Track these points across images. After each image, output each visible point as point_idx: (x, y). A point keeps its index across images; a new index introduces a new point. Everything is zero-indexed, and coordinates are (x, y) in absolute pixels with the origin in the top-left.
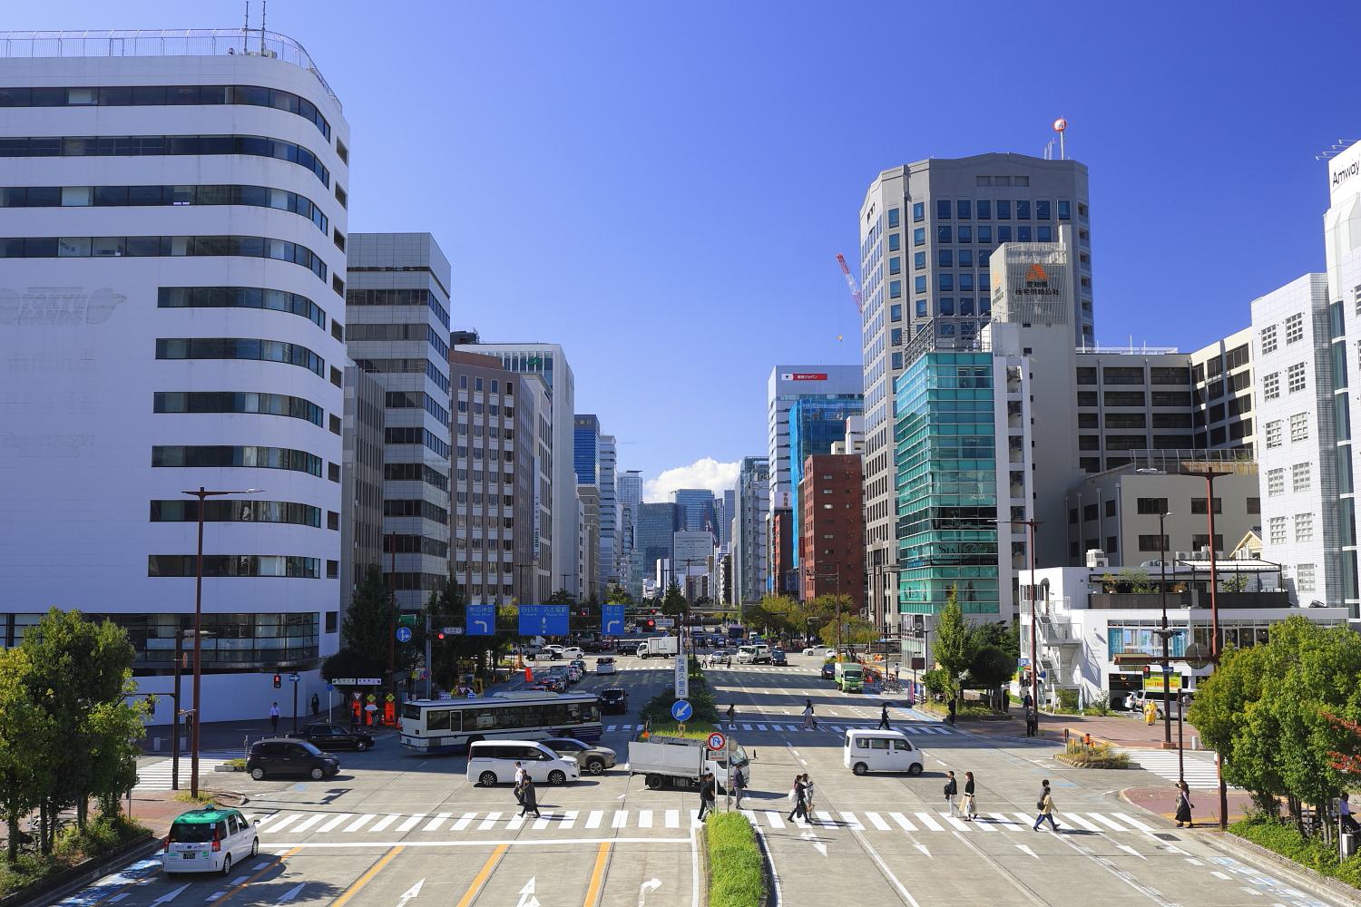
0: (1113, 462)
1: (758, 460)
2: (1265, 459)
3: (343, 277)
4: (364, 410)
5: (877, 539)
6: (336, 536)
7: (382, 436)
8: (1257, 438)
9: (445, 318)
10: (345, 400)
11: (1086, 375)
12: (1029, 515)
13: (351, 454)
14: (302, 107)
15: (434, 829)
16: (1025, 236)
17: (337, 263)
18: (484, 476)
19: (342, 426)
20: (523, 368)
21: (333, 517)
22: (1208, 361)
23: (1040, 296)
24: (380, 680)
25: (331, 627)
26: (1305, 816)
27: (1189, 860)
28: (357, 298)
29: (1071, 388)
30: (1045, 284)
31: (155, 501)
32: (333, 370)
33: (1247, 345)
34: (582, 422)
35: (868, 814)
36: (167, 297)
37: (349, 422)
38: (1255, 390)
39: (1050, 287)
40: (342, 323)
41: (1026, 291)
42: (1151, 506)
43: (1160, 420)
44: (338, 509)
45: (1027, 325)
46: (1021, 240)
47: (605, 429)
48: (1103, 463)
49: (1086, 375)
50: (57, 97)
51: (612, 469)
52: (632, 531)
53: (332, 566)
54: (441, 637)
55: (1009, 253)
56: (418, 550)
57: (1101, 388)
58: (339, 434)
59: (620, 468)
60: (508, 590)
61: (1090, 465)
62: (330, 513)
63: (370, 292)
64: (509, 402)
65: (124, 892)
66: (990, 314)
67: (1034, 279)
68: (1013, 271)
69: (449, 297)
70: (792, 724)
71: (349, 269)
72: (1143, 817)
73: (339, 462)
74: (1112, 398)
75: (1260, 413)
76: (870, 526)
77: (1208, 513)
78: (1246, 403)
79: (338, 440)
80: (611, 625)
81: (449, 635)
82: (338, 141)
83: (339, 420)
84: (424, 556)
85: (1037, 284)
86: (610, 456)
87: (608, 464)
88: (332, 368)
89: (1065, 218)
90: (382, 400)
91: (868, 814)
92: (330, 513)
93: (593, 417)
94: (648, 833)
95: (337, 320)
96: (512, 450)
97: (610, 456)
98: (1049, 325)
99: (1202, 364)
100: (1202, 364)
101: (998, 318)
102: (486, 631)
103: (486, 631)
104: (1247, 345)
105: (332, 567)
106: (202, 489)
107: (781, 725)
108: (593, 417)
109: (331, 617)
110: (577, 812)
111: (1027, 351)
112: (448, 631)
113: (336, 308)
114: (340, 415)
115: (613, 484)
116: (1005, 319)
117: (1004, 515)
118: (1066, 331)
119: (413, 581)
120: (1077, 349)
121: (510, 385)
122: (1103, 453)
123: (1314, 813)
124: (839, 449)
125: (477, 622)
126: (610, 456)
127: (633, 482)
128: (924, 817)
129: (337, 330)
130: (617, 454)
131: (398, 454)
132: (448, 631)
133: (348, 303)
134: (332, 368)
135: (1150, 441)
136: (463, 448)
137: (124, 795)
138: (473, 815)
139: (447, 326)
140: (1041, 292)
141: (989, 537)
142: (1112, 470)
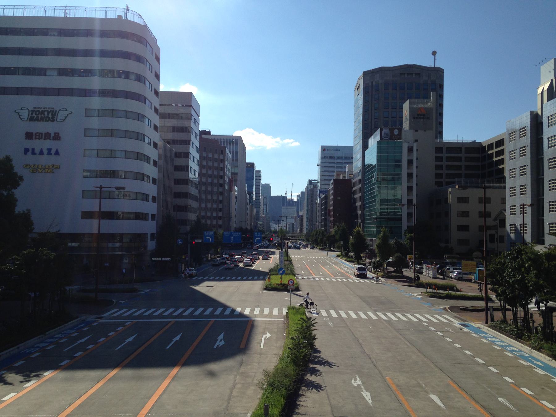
1: (313, 180)
2: (509, 183)
3: (158, 107)
6: (155, 205)
8: (507, 174)
9: (198, 124)
11: (439, 150)
12: (415, 202)
14: (122, 35)
15: (208, 314)
16: (417, 97)
17: (156, 102)
18: (211, 193)
20: (227, 145)
21: (154, 198)
22: (495, 142)
23: (422, 120)
24: (170, 258)
25: (152, 239)
26: (519, 320)
27: (472, 334)
28: (163, 116)
33: (504, 139)
34: (249, 165)
35: (349, 312)
37: (160, 163)
38: (506, 156)
40: (158, 125)
41: (417, 118)
42: (462, 200)
43: (467, 167)
44: (156, 195)
45: (416, 131)
46: (416, 98)
47: (258, 167)
52: (267, 206)
54: (194, 243)
55: (410, 103)
56: (186, 211)
58: (156, 167)
59: (263, 182)
60: (220, 226)
61: (439, 184)
62: (153, 197)
63: (169, 114)
64: (222, 157)
65: (39, 352)
66: (402, 127)
68: (411, 110)
69: (199, 117)
70: (322, 278)
71: (160, 105)
72: (456, 317)
75: (508, 166)
77: (483, 203)
78: (502, 161)
80: (257, 240)
81: (197, 242)
82: (156, 54)
83: (157, 162)
84: (189, 213)
86: (259, 178)
87: (258, 181)
89: (433, 90)
91: (349, 312)
93: (253, 163)
96: (222, 175)
97: (259, 178)
98: (425, 131)
99: (493, 143)
100: (493, 143)
101: (405, 128)
102: (210, 241)
103: (210, 241)
104: (504, 139)
105: (153, 216)
106: (101, 186)
107: (324, 278)
108: (253, 163)
110: (241, 308)
111: (416, 141)
112: (196, 241)
113: (156, 120)
114: (157, 159)
115: (260, 188)
116: (408, 129)
119: (184, 222)
120: (436, 140)
121: (222, 151)
123: (523, 319)
124: (343, 177)
125: (207, 238)
126: (259, 178)
127: (267, 187)
128: (371, 314)
131: (179, 175)
132: (196, 241)
133: (160, 118)
136: (204, 174)
137: (339, 253)
139: (198, 128)
141: (399, 211)
142: (447, 186)
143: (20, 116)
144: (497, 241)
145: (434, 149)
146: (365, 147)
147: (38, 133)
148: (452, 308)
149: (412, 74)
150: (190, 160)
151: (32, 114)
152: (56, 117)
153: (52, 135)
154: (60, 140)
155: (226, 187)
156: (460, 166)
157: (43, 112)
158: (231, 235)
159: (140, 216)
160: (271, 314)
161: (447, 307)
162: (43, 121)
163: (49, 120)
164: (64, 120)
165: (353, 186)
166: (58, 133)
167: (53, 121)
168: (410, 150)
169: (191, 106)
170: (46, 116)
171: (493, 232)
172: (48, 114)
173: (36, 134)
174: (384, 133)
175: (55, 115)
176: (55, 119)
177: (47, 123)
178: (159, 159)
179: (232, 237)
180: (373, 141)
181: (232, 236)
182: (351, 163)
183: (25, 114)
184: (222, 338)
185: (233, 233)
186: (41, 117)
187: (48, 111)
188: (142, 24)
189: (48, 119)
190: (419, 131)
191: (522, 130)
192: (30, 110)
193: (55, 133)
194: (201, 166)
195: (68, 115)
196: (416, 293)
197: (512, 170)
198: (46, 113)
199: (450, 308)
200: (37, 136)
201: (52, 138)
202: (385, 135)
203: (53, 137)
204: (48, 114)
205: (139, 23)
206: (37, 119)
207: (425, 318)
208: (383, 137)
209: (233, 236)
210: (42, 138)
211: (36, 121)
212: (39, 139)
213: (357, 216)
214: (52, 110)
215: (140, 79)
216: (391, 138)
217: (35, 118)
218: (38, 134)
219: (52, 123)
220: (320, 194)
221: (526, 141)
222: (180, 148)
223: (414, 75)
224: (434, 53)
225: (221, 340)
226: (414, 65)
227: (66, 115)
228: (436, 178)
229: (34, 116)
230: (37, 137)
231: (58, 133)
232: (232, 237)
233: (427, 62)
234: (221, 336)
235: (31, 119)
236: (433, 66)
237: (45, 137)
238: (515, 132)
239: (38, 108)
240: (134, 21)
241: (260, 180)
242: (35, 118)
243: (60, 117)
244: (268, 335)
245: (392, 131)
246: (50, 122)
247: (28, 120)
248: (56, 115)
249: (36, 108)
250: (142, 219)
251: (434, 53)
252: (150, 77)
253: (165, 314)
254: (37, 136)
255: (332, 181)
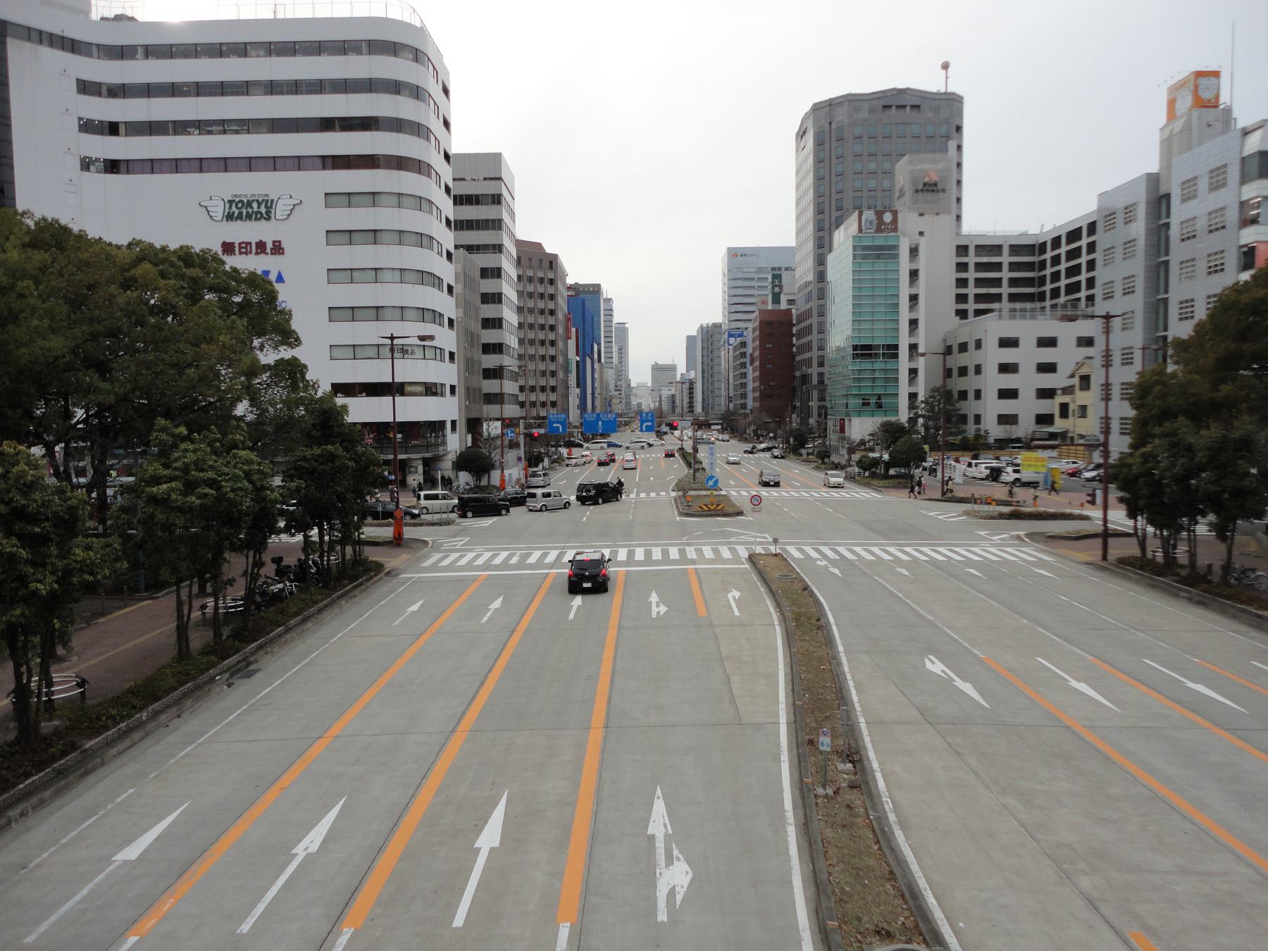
0: (978, 313)
3: (451, 184)
4: (465, 277)
5: (804, 368)
7: (479, 299)
10: (456, 273)
11: (962, 250)
13: (461, 311)
14: (392, 49)
15: (534, 562)
17: (446, 173)
19: (455, 291)
28: (459, 200)
29: (951, 259)
30: (936, 185)
31: (957, 252)
32: (449, 285)
36: (331, 198)
39: (940, 187)
40: (452, 219)
41: (922, 190)
44: (454, 350)
45: (921, 215)
48: (971, 313)
49: (962, 250)
50: (242, 50)
51: (611, 321)
53: (453, 388)
57: (972, 259)
59: (617, 319)
62: (450, 352)
64: (551, 275)
67: (927, 180)
71: (454, 180)
73: (453, 317)
74: (980, 267)
76: (798, 358)
79: (451, 301)
85: (930, 185)
88: (448, 284)
90: (478, 273)
92: (450, 352)
94: (657, 563)
95: (449, 249)
109: (454, 423)
111: (921, 234)
114: (453, 284)
117: (904, 352)
118: (949, 219)
121: (551, 263)
122: (971, 306)
125: (555, 425)
129: (448, 222)
130: (614, 310)
134: (448, 284)
135: (1005, 297)
138: (557, 552)
140: (933, 191)
143: (208, 211)
144: (1073, 416)
145: (954, 249)
146: (823, 245)
147: (243, 243)
148: (1031, 536)
149: (904, 107)
150: (504, 283)
151: (230, 208)
152: (273, 212)
153: (269, 246)
154: (283, 253)
155: (561, 330)
156: (1000, 280)
157: (249, 204)
158: (598, 419)
159: (431, 390)
160: (648, 559)
161: (1021, 533)
162: (250, 220)
163: (262, 216)
164: (288, 215)
165: (794, 322)
166: (279, 242)
167: (268, 218)
168: (914, 251)
169: (500, 179)
170: (256, 209)
171: (1066, 399)
172: (259, 207)
173: (240, 244)
174: (866, 221)
175: (271, 207)
176: (273, 216)
177: (258, 222)
178: (456, 282)
179: (600, 423)
180: (844, 238)
181: (600, 419)
182: (494, 246)
183: (219, 210)
184: (657, 599)
185: (601, 416)
186: (248, 212)
187: (257, 201)
188: (418, 24)
189: (259, 216)
190: (926, 216)
191: (1129, 210)
192: (226, 201)
193: (274, 242)
194: (520, 294)
195: (294, 205)
196: (951, 514)
197: (1128, 292)
198: (255, 205)
199: (1028, 535)
200: (243, 248)
201: (268, 251)
202: (868, 224)
203: (271, 249)
204: (259, 207)
205: (413, 23)
206: (240, 217)
207: (976, 553)
208: (863, 228)
209: (602, 421)
210: (251, 252)
211: (239, 221)
212: (246, 253)
213: (805, 379)
214: (266, 198)
215: (418, 130)
216: (878, 230)
217: (236, 215)
218: (244, 245)
219: (267, 222)
220: (730, 339)
221: (1139, 229)
222: (486, 260)
223: (908, 108)
224: (945, 66)
225: (657, 603)
226: (907, 89)
227: (292, 207)
228: (957, 302)
229: (234, 212)
230: (243, 250)
231: (279, 242)
232: (600, 423)
233: (930, 82)
234: (654, 598)
235: (230, 217)
236: (943, 91)
237: (257, 250)
238: (1114, 213)
239: (240, 196)
240: (404, 20)
241: (611, 315)
242: (236, 215)
243: (280, 210)
244: (737, 594)
245: (879, 214)
246: (263, 221)
247: (225, 219)
248: (274, 207)
249: (236, 196)
250: (435, 394)
251: (945, 66)
252: (436, 126)
253: (459, 564)
254: (243, 248)
255: (757, 313)
